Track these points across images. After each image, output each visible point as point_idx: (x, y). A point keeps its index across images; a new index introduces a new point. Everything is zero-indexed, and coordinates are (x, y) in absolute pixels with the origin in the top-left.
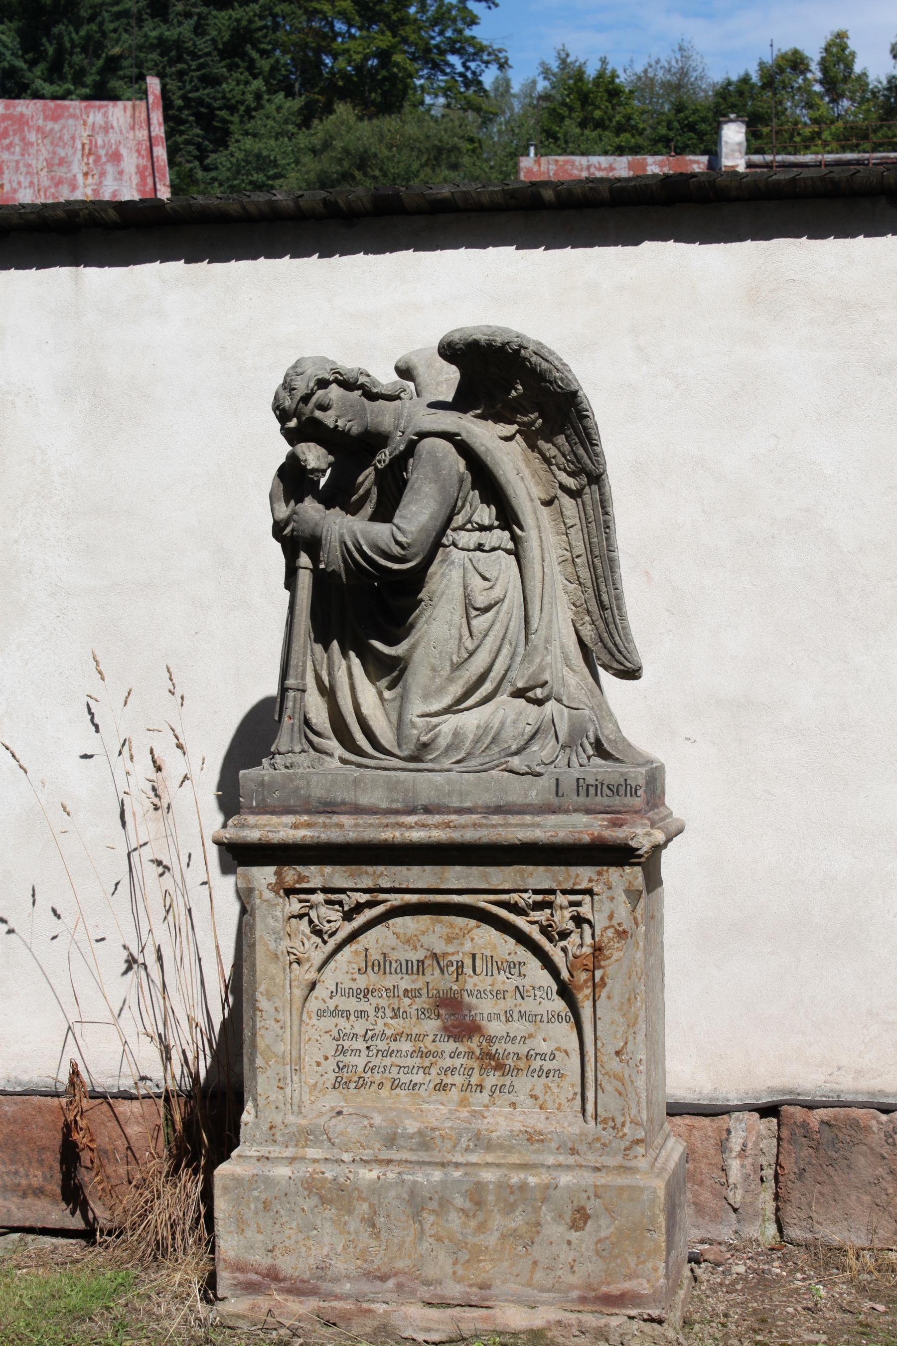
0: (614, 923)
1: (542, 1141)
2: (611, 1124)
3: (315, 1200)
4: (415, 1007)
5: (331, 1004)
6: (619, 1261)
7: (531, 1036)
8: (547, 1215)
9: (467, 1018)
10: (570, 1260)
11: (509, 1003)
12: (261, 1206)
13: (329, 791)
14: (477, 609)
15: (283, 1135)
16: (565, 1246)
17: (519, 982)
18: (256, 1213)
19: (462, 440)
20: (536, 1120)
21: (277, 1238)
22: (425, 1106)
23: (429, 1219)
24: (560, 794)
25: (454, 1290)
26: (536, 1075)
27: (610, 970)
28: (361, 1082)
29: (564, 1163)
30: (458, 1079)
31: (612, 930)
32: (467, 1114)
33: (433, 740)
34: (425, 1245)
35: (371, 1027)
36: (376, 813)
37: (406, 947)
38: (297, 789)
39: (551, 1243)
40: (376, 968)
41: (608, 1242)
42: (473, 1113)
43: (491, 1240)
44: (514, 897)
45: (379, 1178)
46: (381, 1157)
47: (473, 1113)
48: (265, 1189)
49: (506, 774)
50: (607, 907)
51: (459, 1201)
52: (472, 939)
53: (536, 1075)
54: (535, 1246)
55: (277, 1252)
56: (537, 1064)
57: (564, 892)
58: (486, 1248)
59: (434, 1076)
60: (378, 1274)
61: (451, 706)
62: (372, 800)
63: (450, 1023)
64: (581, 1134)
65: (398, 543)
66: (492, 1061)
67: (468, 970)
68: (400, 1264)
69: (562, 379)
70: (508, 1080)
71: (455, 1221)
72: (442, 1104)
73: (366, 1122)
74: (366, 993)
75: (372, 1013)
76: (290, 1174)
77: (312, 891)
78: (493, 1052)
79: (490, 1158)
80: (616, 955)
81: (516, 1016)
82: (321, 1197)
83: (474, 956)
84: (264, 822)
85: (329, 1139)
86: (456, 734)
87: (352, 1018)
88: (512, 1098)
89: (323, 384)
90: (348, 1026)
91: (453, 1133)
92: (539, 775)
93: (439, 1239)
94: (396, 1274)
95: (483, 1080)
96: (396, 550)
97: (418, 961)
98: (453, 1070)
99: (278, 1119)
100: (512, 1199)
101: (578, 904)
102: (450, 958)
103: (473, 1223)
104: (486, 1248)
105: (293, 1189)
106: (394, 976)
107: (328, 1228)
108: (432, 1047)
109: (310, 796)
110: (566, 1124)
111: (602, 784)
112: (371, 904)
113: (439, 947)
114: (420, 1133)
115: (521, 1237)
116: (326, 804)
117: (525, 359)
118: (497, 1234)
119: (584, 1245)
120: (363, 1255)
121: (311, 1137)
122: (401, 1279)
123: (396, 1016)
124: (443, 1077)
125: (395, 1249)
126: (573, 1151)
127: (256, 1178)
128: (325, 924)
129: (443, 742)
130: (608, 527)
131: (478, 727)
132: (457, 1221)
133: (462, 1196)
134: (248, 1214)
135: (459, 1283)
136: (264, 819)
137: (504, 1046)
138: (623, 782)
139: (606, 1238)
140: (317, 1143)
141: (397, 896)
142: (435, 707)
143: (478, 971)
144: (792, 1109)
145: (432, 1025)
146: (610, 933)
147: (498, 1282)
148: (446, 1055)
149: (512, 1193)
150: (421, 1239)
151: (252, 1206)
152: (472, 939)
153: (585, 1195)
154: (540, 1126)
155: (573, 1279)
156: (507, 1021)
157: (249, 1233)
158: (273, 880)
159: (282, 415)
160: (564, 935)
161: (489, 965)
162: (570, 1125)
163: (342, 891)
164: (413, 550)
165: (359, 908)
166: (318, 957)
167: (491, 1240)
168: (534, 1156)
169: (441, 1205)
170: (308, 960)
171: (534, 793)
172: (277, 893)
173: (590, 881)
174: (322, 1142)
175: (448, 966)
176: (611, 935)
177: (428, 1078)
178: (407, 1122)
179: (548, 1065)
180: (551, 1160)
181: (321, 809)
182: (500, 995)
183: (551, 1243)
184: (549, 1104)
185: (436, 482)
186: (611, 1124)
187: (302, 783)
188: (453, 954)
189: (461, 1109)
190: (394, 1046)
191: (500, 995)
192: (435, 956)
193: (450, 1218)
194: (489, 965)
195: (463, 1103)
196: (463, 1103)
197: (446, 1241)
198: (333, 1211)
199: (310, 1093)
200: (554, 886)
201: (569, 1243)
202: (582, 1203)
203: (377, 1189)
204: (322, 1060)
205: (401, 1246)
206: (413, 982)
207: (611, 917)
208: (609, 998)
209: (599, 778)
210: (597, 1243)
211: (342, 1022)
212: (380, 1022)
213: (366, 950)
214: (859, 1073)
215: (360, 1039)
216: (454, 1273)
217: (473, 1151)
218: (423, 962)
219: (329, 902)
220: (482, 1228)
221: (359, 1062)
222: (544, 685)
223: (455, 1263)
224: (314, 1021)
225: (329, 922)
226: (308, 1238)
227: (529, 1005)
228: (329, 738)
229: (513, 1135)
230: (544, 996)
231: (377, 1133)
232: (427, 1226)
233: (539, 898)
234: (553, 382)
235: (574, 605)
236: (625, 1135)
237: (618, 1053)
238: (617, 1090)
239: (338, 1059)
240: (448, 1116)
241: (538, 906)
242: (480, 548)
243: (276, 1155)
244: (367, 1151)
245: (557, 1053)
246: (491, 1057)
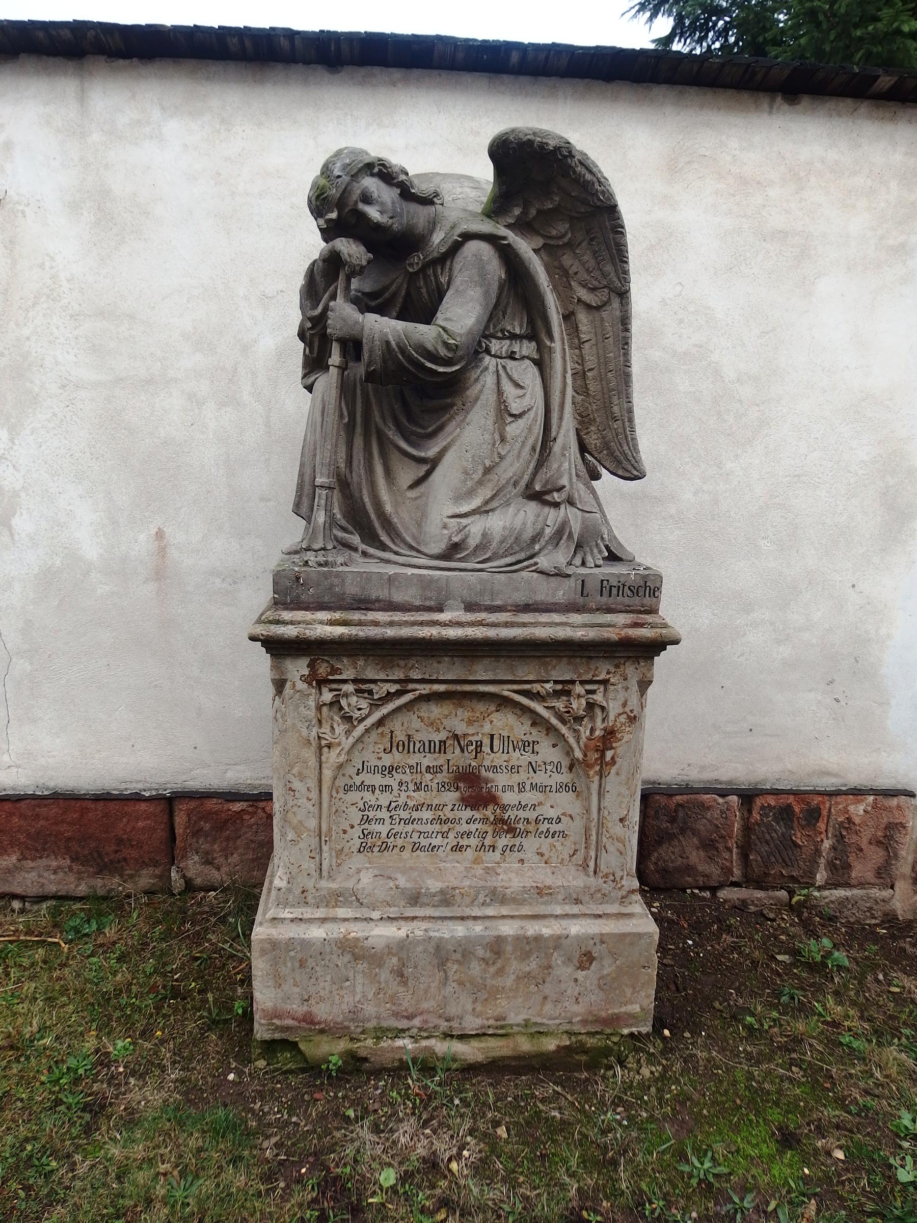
0: (627, 709)
1: (551, 894)
2: (612, 878)
3: (348, 957)
4: (436, 781)
5: (358, 780)
6: (617, 992)
7: (540, 804)
8: (557, 959)
9: (484, 790)
10: (576, 994)
11: (523, 776)
12: (298, 965)
13: (363, 589)
14: (512, 415)
15: (314, 898)
16: (572, 983)
17: (532, 758)
18: (293, 970)
19: (509, 245)
20: (545, 877)
21: (312, 989)
22: (442, 865)
23: (453, 968)
24: (585, 593)
25: (472, 1024)
26: (543, 836)
27: (620, 751)
28: (384, 846)
29: (570, 913)
30: (474, 842)
31: (625, 716)
32: (482, 871)
33: (463, 541)
34: (449, 989)
35: (394, 799)
36: (409, 610)
37: (430, 729)
38: (331, 587)
39: (560, 981)
40: (401, 748)
41: (609, 978)
42: (487, 870)
43: (509, 981)
44: (536, 687)
45: (408, 936)
46: (406, 915)
47: (487, 870)
48: (301, 950)
49: (535, 575)
50: (621, 696)
51: (480, 952)
52: (491, 722)
53: (543, 836)
54: (547, 985)
55: (312, 1001)
56: (544, 827)
57: (583, 683)
58: (503, 988)
59: (452, 840)
60: (405, 1014)
61: (479, 508)
62: (406, 598)
63: (468, 794)
64: (585, 887)
65: (446, 344)
66: (505, 826)
67: (486, 749)
68: (425, 1005)
69: (603, 193)
70: (517, 841)
71: (476, 969)
72: (458, 862)
73: (391, 884)
74: (391, 770)
75: (396, 787)
76: (324, 936)
77: (345, 681)
78: (506, 818)
79: (505, 911)
80: (627, 737)
81: (528, 787)
82: (353, 954)
83: (492, 736)
84: (299, 619)
85: (358, 900)
86: (484, 535)
87: (377, 791)
88: (521, 855)
89: (355, 177)
90: (373, 799)
91: (472, 891)
92: (569, 576)
93: (461, 983)
94: (421, 1014)
95: (496, 841)
96: (443, 352)
97: (440, 742)
98: (469, 834)
99: (310, 884)
100: (528, 948)
101: (593, 692)
102: (470, 738)
103: (492, 970)
104: (503, 988)
105: (328, 949)
106: (418, 755)
107: (360, 979)
108: (450, 815)
109: (344, 594)
110: (571, 878)
111: (624, 585)
112: (400, 693)
113: (461, 728)
114: (442, 892)
115: (534, 978)
116: (360, 601)
117: (570, 166)
118: (513, 977)
119: (588, 982)
120: (393, 999)
121: (341, 899)
122: (425, 1017)
123: (418, 789)
124: (459, 839)
125: (421, 993)
126: (577, 901)
127: (292, 941)
128: (356, 711)
129: (472, 542)
130: (627, 344)
131: (504, 528)
132: (478, 968)
133: (483, 948)
134: (284, 971)
135: (478, 1017)
136: (299, 615)
137: (516, 812)
138: (642, 583)
139: (608, 975)
140: (347, 904)
141: (425, 686)
142: (465, 509)
143: (495, 749)
144: (658, 797)
145: (451, 797)
146: (623, 719)
147: (512, 1015)
148: (463, 821)
149: (528, 943)
150: (445, 984)
151: (289, 965)
152: (491, 722)
153: (592, 942)
154: (549, 882)
155: (576, 1008)
156: (520, 791)
157: (286, 987)
158: (306, 672)
159: (319, 203)
160: (578, 719)
161: (506, 744)
162: (574, 879)
163: (374, 681)
164: (460, 353)
165: (389, 697)
166: (347, 743)
167: (509, 981)
168: (543, 907)
169: (463, 956)
170: (339, 744)
171: (561, 593)
172: (310, 684)
173: (608, 673)
174: (351, 902)
175: (467, 745)
176: (624, 721)
177: (446, 841)
178: (429, 882)
179: (554, 827)
180: (558, 911)
181: (355, 606)
182: (514, 769)
183: (560, 981)
184: (554, 859)
185: (481, 286)
186: (612, 878)
187: (336, 581)
188: (473, 735)
189: (475, 866)
190: (415, 815)
191: (514, 769)
192: (456, 737)
193: (471, 966)
194: (506, 744)
195: (477, 861)
196: (477, 861)
197: (468, 985)
198: (365, 965)
199: (337, 857)
200: (575, 677)
201: (576, 980)
202: (589, 949)
203: (402, 947)
204: (348, 829)
205: (426, 991)
206: (435, 759)
207: (625, 705)
208: (618, 774)
209: (621, 580)
210: (599, 979)
211: (368, 796)
212: (403, 794)
213: (392, 732)
214: (703, 768)
215: (384, 810)
216: (474, 1009)
217: (489, 905)
218: (445, 742)
219: (358, 691)
220: (500, 972)
221: (384, 829)
222: (560, 489)
223: (475, 1001)
224: (341, 795)
225: (359, 709)
226: (341, 988)
227: (540, 778)
228: (351, 533)
229: (525, 890)
230: (554, 770)
231: (403, 893)
232: (450, 974)
233: (559, 687)
234: (595, 194)
235: (579, 415)
236: (623, 886)
237: (621, 820)
238: (618, 850)
239: (363, 827)
240: (465, 874)
241: (557, 694)
242: (512, 356)
243: (309, 916)
244: (392, 909)
245: (562, 817)
246: (503, 822)
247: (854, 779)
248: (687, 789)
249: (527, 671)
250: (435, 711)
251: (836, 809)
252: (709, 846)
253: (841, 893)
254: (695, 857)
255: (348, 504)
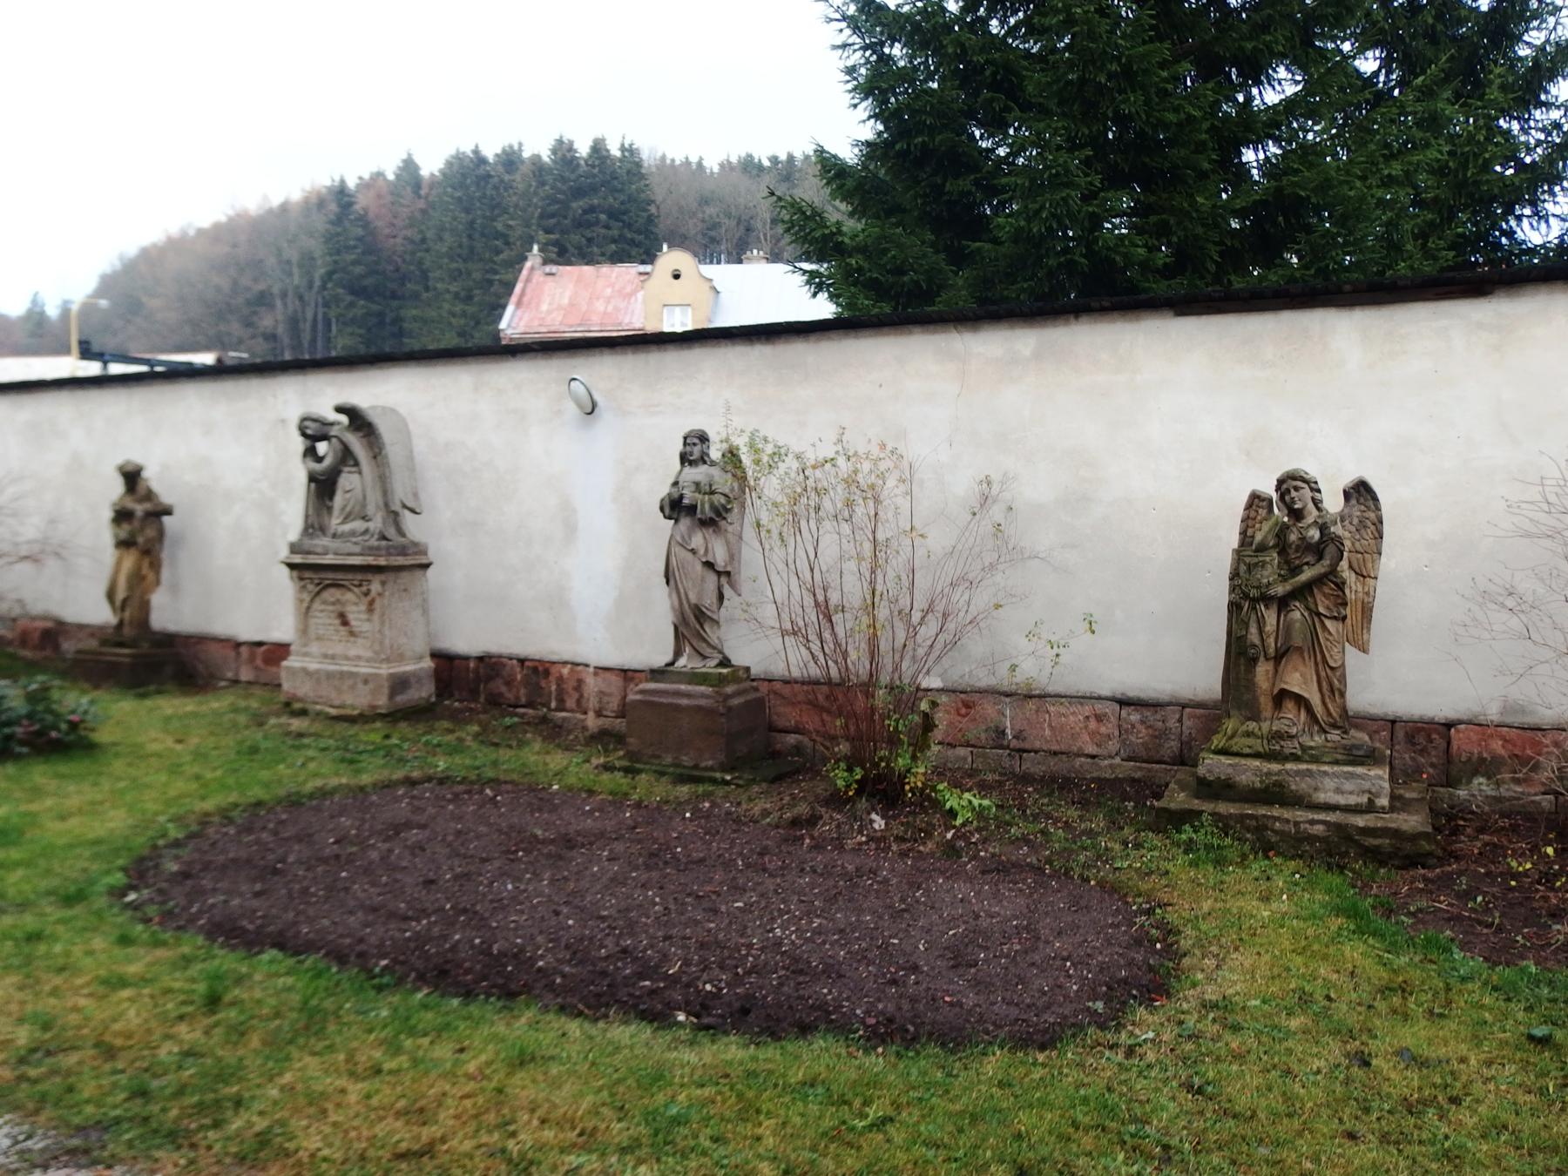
13: (693, 625)
20: (361, 652)
25: (337, 702)
66: (352, 634)
203: (317, 672)
247: (566, 657)
248: (500, 656)
249: (350, 576)
250: (332, 590)
251: (554, 670)
252: (509, 683)
253: (564, 714)
254: (503, 689)
255: (314, 526)
